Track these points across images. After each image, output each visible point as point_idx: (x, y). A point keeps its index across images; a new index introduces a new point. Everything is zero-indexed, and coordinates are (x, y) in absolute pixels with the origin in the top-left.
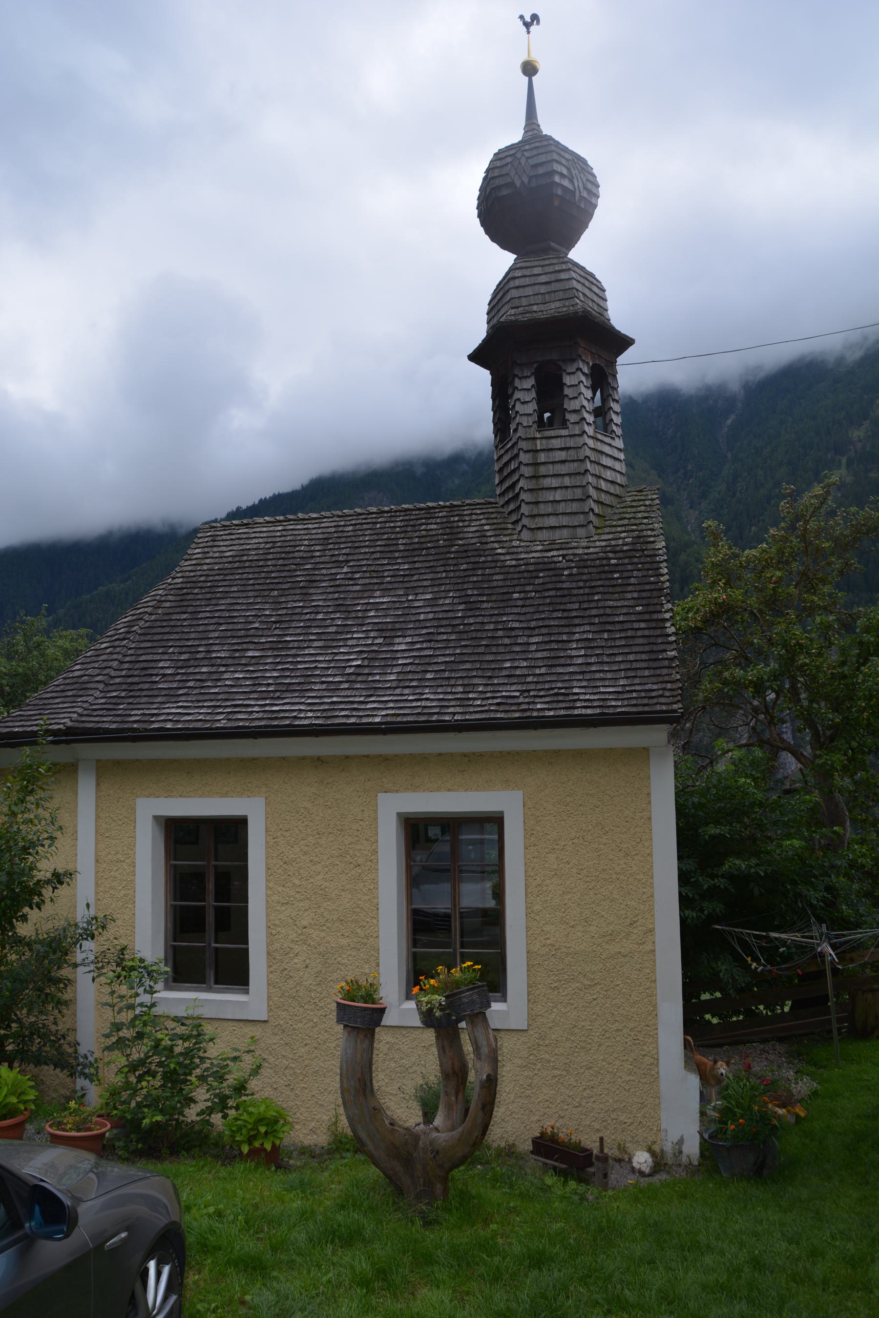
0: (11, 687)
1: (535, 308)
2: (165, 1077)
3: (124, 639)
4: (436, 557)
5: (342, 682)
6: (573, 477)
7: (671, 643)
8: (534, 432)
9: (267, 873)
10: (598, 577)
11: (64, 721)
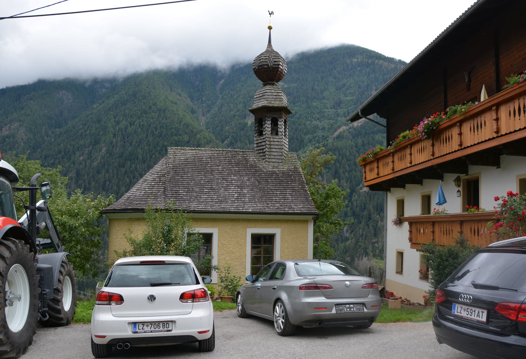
8: (270, 136)
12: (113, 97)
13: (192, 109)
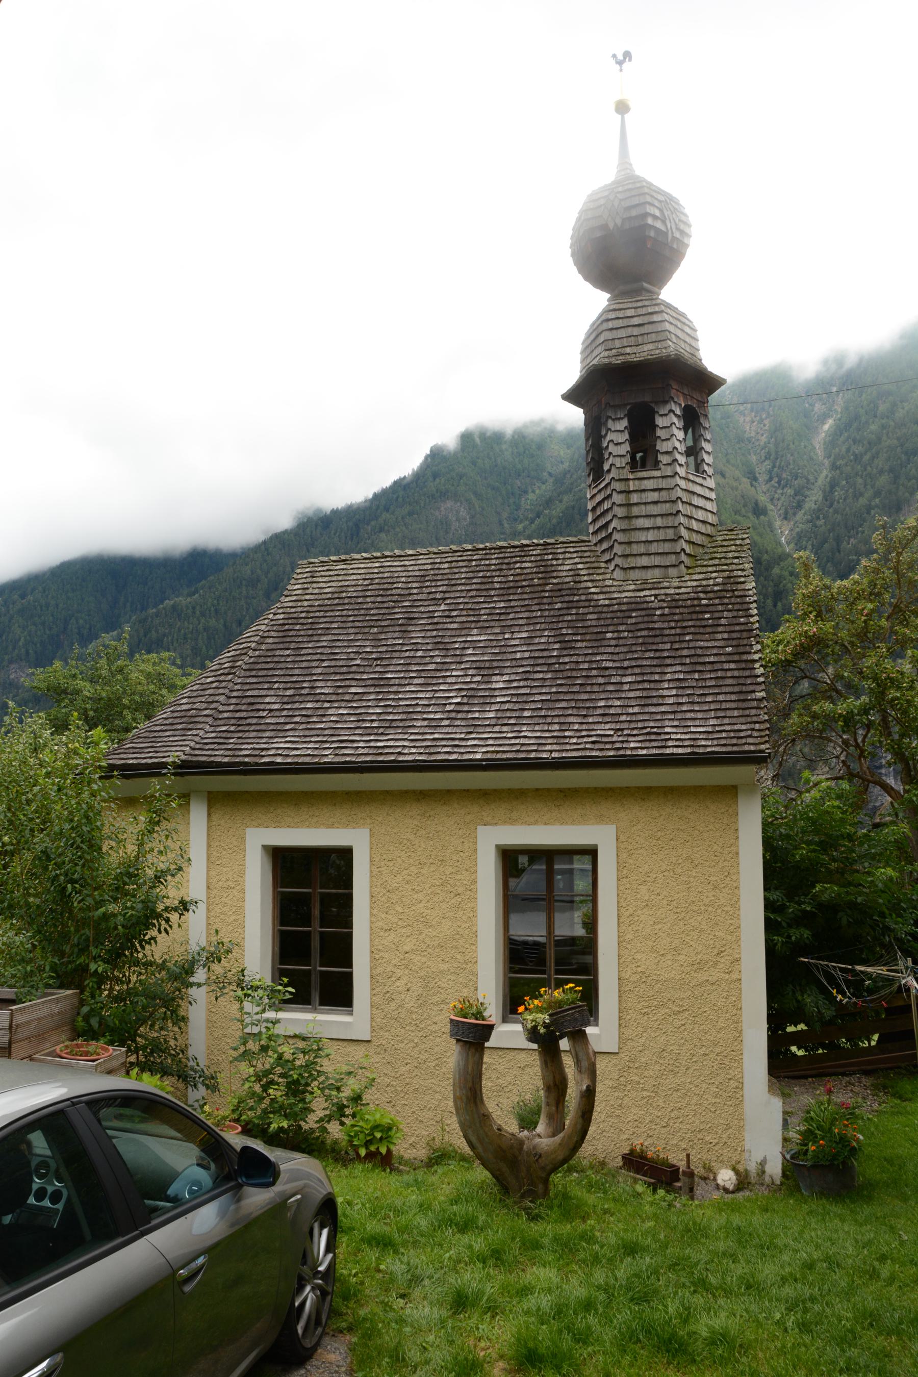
0: (95, 711)
1: (628, 350)
2: (288, 1085)
3: (229, 674)
4: (531, 596)
5: (443, 719)
6: (665, 517)
7: (760, 684)
8: (626, 474)
9: (371, 901)
10: (689, 617)
11: (174, 755)
12: (561, 501)
13: (756, 504)
